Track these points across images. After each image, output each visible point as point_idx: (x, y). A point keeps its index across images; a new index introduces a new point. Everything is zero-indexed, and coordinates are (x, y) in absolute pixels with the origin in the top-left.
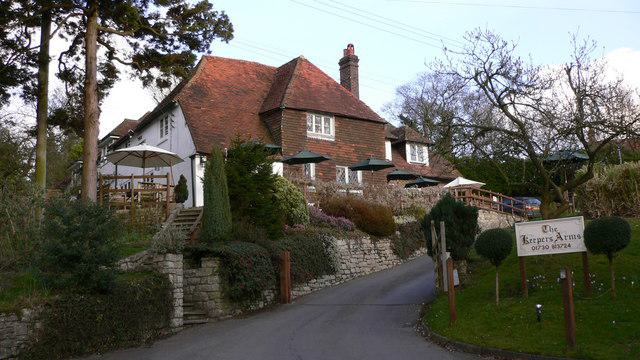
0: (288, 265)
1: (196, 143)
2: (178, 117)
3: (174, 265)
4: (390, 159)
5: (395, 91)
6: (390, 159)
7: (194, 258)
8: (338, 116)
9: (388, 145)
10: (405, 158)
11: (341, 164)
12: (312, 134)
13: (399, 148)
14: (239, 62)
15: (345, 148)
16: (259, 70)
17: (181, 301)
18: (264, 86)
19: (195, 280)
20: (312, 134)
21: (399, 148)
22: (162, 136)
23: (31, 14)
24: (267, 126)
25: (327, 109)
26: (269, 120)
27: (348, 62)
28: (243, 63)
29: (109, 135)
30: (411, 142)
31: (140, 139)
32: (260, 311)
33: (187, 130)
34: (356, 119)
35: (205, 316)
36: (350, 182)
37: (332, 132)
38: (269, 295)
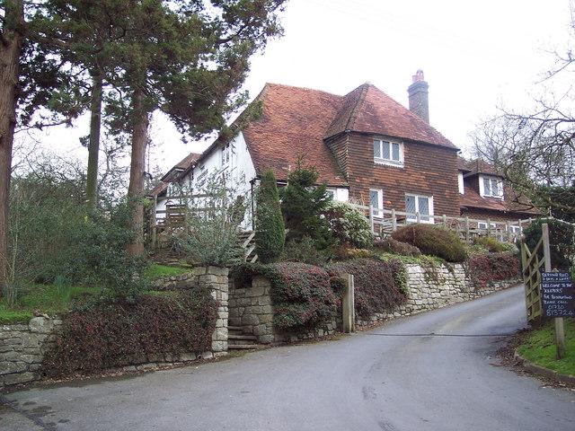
0: (352, 289)
1: (258, 170)
2: (240, 142)
3: (220, 288)
4: (463, 193)
5: (419, 68)
6: (463, 193)
7: (243, 279)
8: (408, 142)
9: (460, 179)
10: (478, 192)
11: (411, 191)
12: (379, 159)
13: (471, 181)
14: (304, 90)
15: (415, 176)
16: (325, 98)
17: (226, 322)
18: (330, 112)
19: (244, 301)
20: (379, 159)
21: (471, 181)
22: (223, 164)
23: (150, 74)
24: (331, 152)
25: (396, 133)
26: (334, 146)
27: (418, 90)
28: (308, 91)
29: (174, 168)
30: (484, 174)
31: (202, 169)
32: (322, 339)
33: (247, 154)
34: (431, 154)
35: (255, 341)
36: (424, 213)
37: (402, 159)
38: (332, 325)
